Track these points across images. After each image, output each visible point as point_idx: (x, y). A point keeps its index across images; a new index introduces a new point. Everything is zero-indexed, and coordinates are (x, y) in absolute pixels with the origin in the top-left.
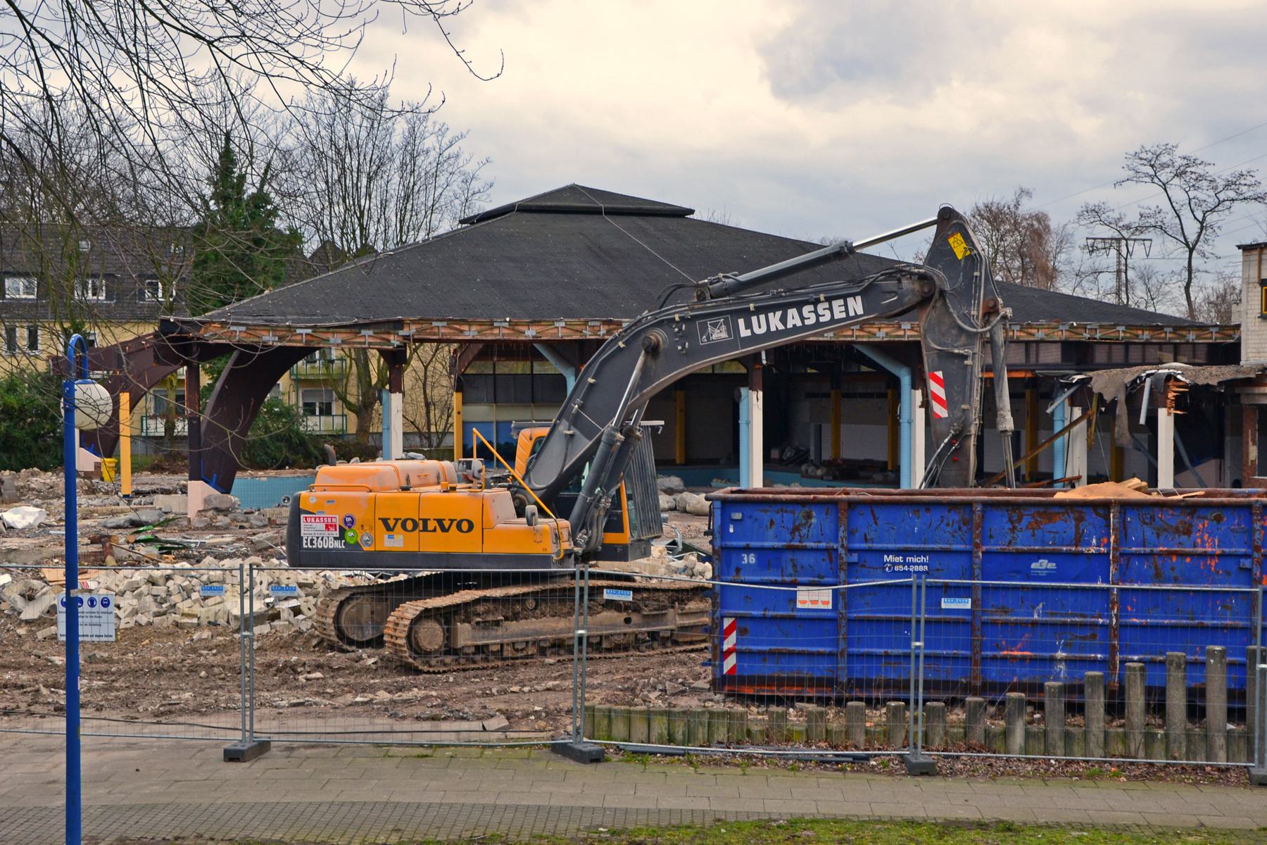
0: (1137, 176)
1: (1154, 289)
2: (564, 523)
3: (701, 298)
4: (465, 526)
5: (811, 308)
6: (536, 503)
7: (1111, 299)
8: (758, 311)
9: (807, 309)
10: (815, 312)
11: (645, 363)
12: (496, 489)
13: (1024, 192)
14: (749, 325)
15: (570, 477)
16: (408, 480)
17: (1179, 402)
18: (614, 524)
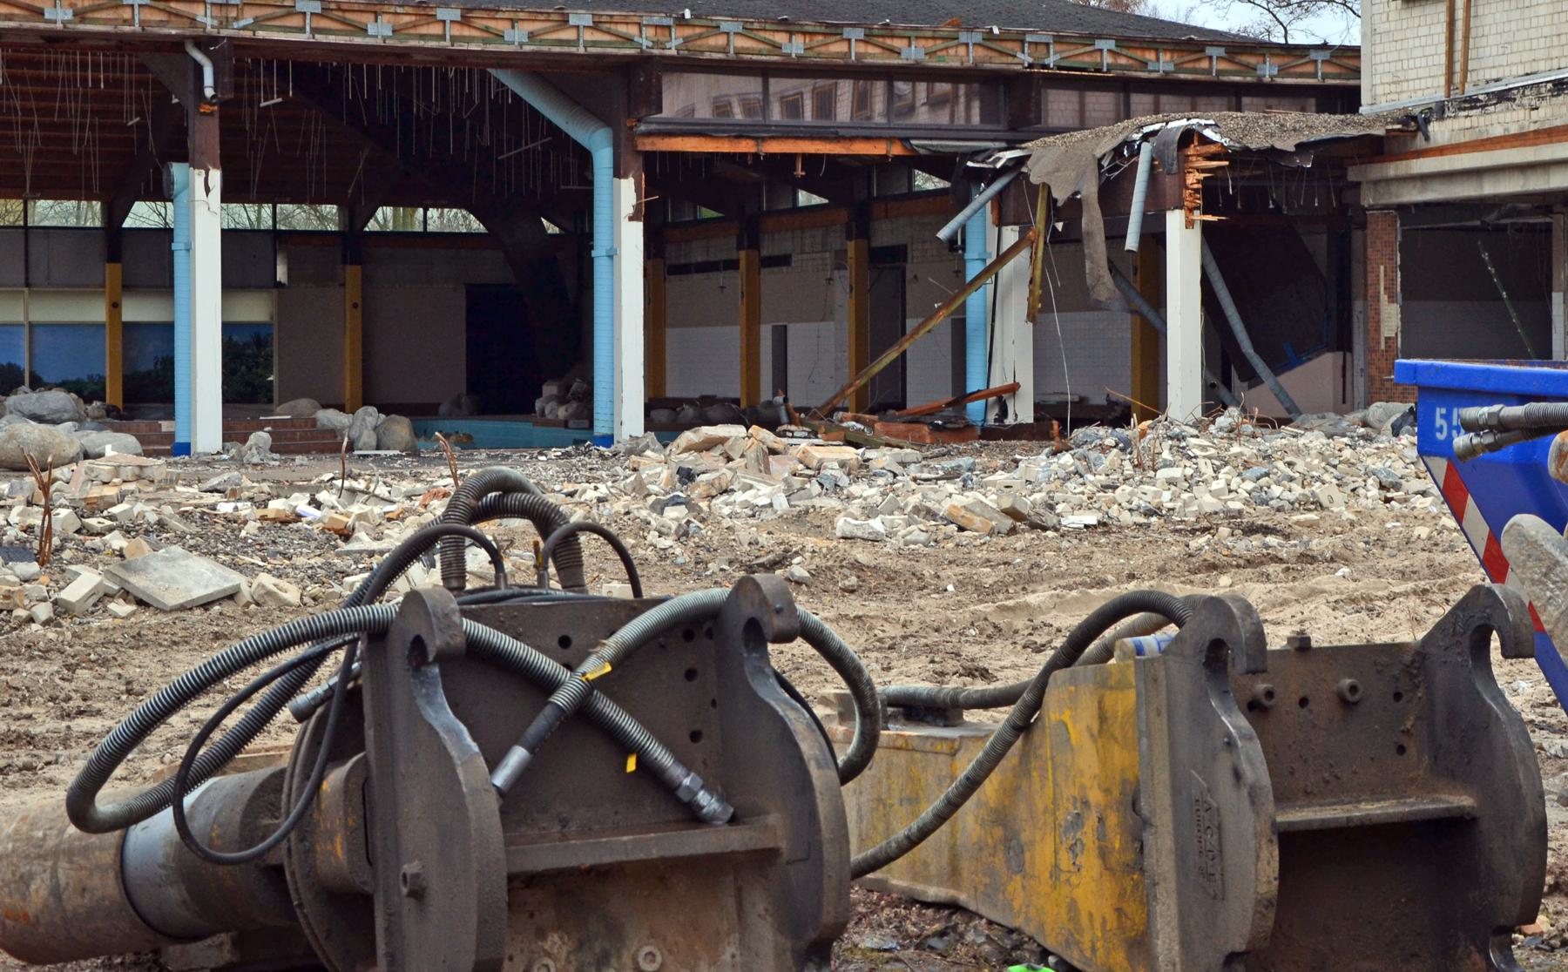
17: (1211, 195)
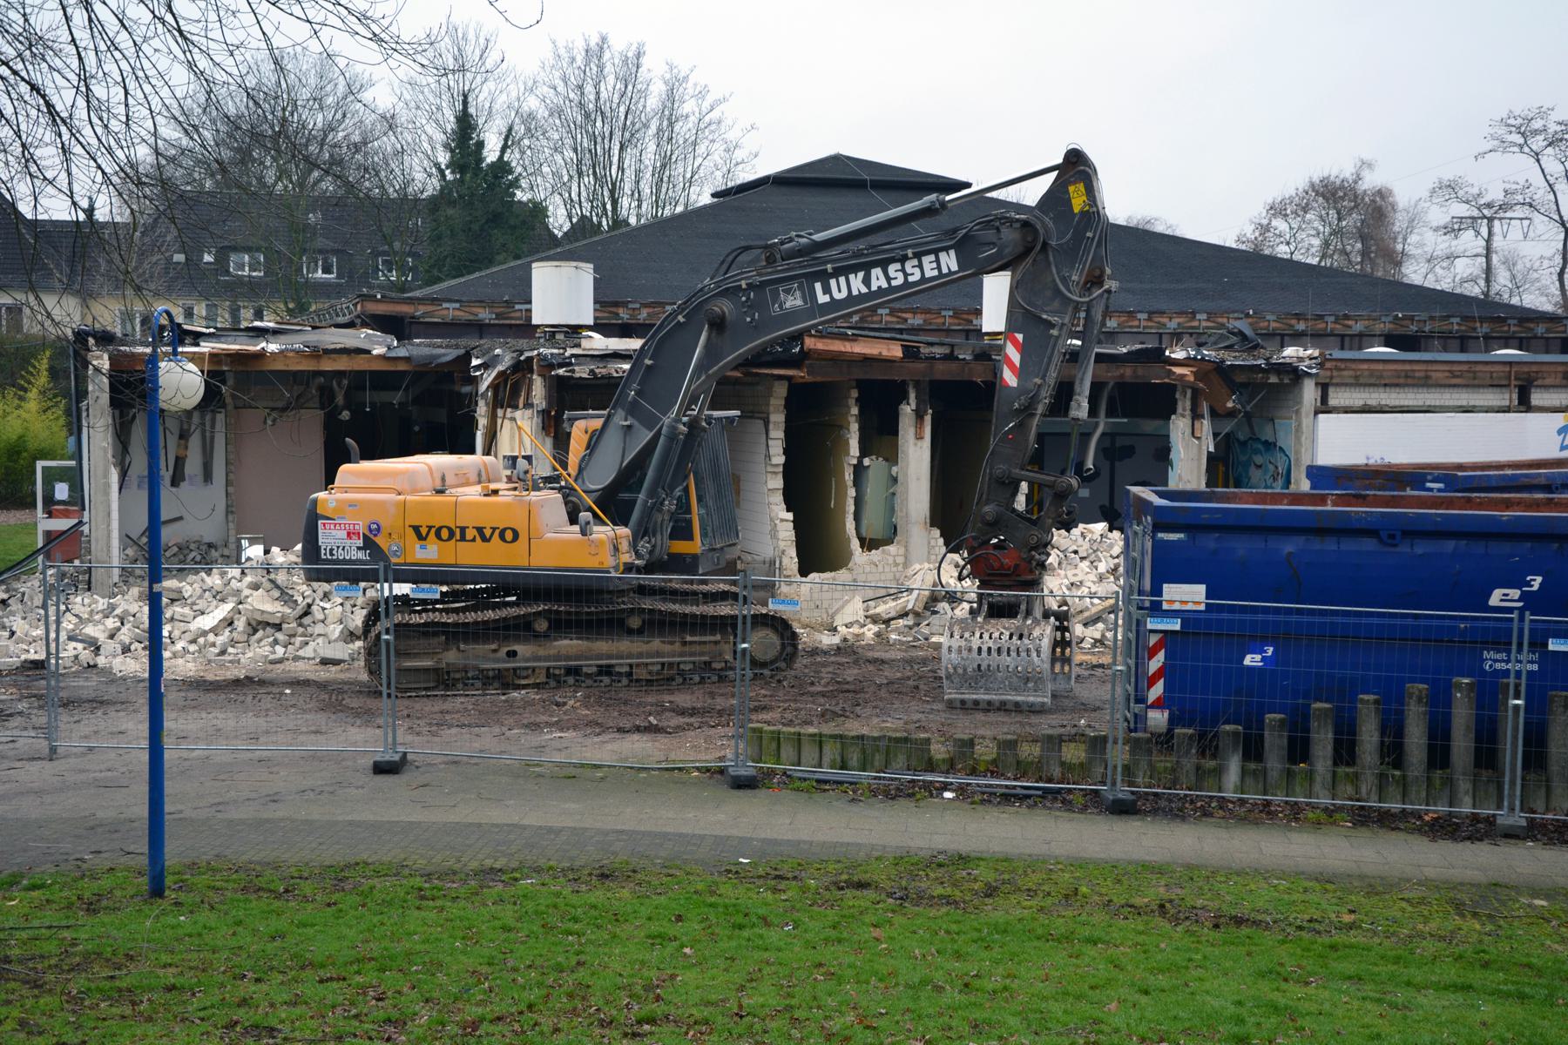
0: (1504, 146)
1: (1519, 277)
2: (624, 531)
3: (771, 260)
4: (509, 535)
5: (898, 266)
6: (590, 509)
7: (1475, 291)
8: (837, 273)
9: (893, 269)
10: (903, 270)
11: (709, 339)
12: (545, 492)
13: (1366, 164)
14: (827, 290)
15: (629, 477)
16: (443, 479)
18: (682, 531)
